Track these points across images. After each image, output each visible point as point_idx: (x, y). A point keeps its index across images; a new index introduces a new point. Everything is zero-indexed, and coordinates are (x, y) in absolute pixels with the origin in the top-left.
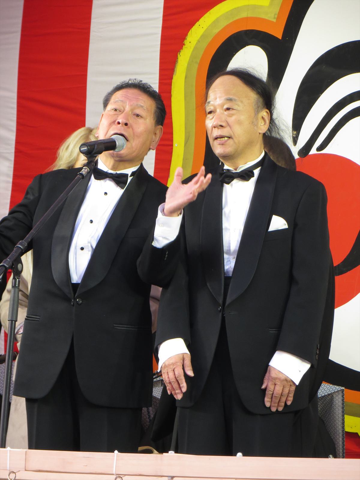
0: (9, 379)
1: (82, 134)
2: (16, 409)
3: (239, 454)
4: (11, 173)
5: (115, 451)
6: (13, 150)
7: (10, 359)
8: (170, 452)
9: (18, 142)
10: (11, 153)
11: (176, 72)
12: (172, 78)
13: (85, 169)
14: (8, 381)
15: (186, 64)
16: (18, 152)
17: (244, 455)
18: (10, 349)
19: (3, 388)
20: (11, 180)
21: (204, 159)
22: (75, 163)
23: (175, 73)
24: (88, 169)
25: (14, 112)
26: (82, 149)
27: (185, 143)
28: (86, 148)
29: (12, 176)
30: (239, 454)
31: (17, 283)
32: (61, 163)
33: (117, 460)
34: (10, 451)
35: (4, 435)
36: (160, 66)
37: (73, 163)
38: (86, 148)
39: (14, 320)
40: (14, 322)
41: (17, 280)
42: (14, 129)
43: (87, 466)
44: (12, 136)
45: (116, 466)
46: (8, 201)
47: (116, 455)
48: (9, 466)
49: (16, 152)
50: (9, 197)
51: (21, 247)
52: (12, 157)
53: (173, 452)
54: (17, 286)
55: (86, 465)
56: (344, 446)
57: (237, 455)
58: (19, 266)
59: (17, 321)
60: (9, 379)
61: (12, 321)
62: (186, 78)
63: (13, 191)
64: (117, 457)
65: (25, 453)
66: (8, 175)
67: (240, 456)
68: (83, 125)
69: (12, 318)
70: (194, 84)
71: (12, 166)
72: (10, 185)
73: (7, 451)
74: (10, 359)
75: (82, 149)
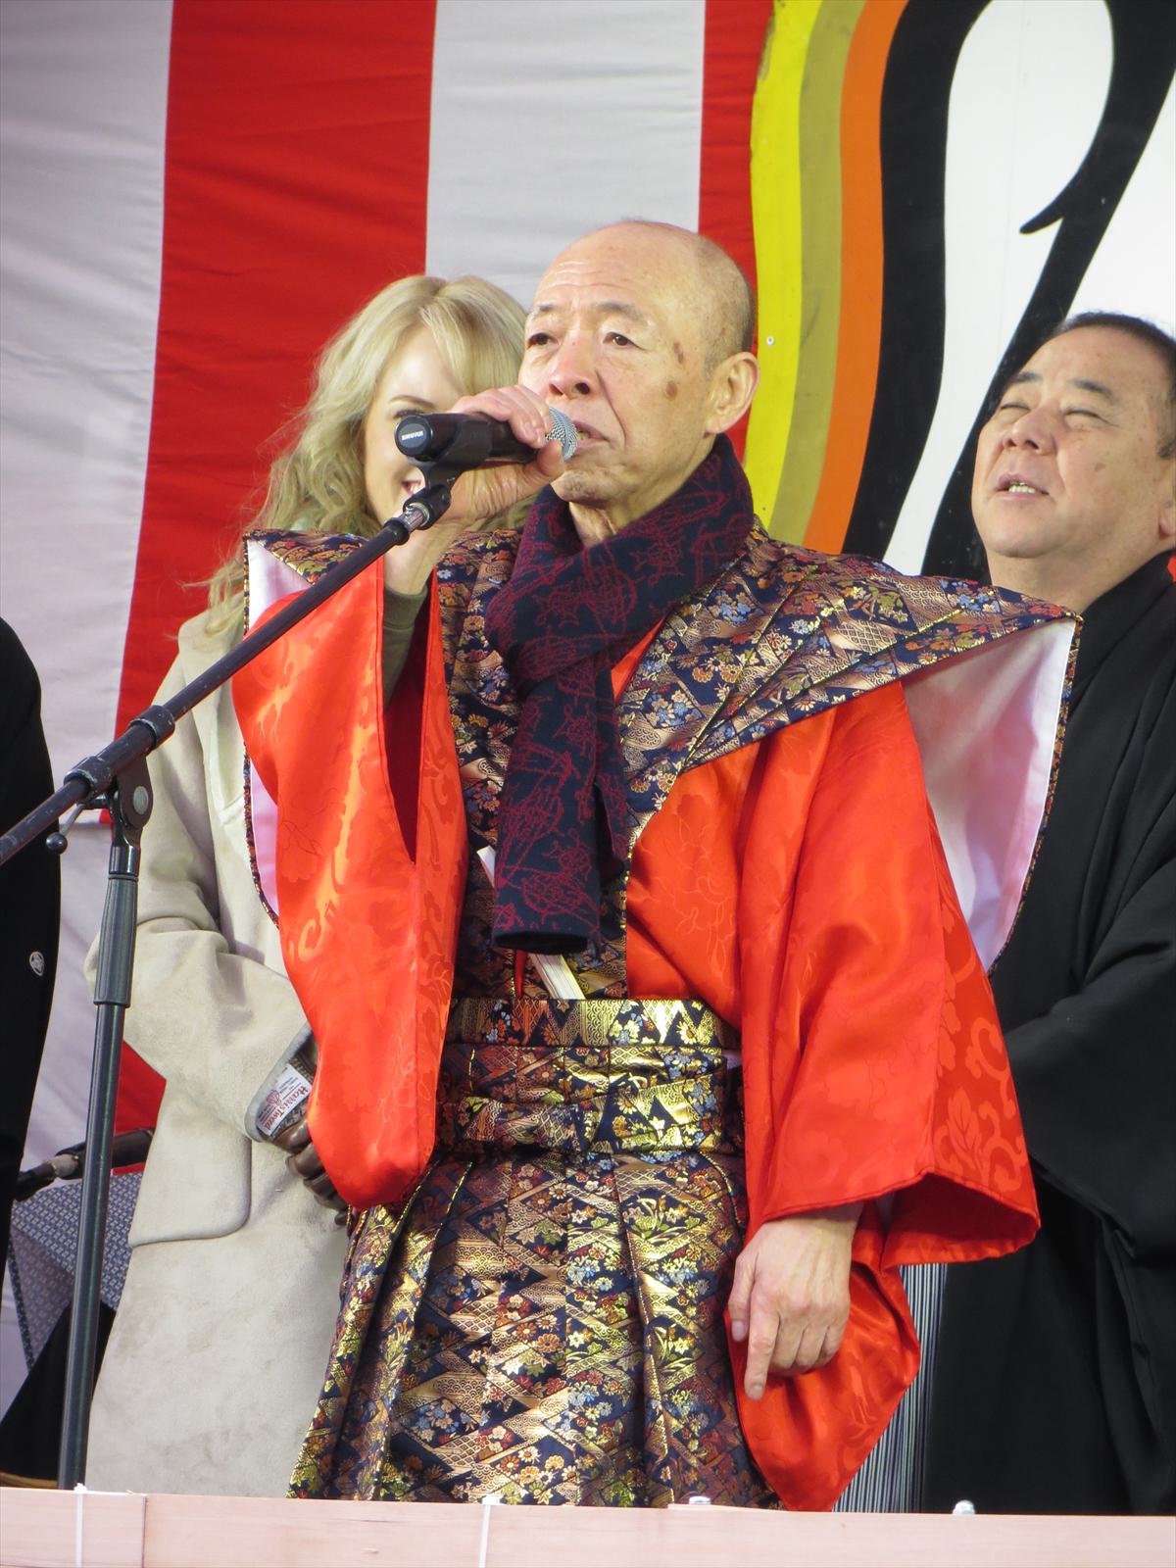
0: (97, 1226)
1: (401, 300)
2: (123, 1347)
3: (964, 1507)
4: (142, 449)
5: (76, 1485)
6: (149, 363)
7: (103, 1151)
8: (693, 1500)
9: (166, 333)
10: (145, 371)
11: (768, 69)
12: (750, 89)
13: (416, 509)
14: (96, 1233)
15: (805, 39)
16: (166, 366)
17: (980, 1509)
18: (103, 1114)
19: (76, 1254)
20: (141, 475)
21: (873, 397)
22: (369, 408)
23: (763, 70)
24: (426, 511)
25: (157, 217)
26: (404, 438)
27: (801, 337)
28: (420, 434)
29: (144, 459)
30: (964, 1507)
31: (130, 858)
32: (319, 408)
33: (491, 1531)
34: (85, 1495)
35: (79, 1440)
36: (708, 44)
37: (362, 409)
38: (420, 434)
39: (119, 1002)
40: (116, 1007)
41: (131, 847)
42: (155, 281)
43: (376, 1553)
44: (145, 309)
45: (487, 1554)
46: (131, 555)
47: (487, 1513)
48: (83, 1553)
49: (160, 370)
50: (134, 542)
51: (151, 724)
52: (145, 388)
53: (705, 1499)
54: (129, 871)
55: (374, 1550)
56: (73, 1260)
57: (954, 1511)
58: (139, 794)
59: (127, 1006)
60: (97, 1226)
61: (109, 1004)
62: (805, 87)
63: (150, 516)
64: (491, 1518)
65: (142, 1507)
66: (129, 459)
67: (965, 1512)
68: (414, 262)
69: (109, 996)
70: (837, 114)
71: (145, 420)
72: (139, 495)
73: (77, 1495)
74: (103, 1151)
75: (404, 438)
